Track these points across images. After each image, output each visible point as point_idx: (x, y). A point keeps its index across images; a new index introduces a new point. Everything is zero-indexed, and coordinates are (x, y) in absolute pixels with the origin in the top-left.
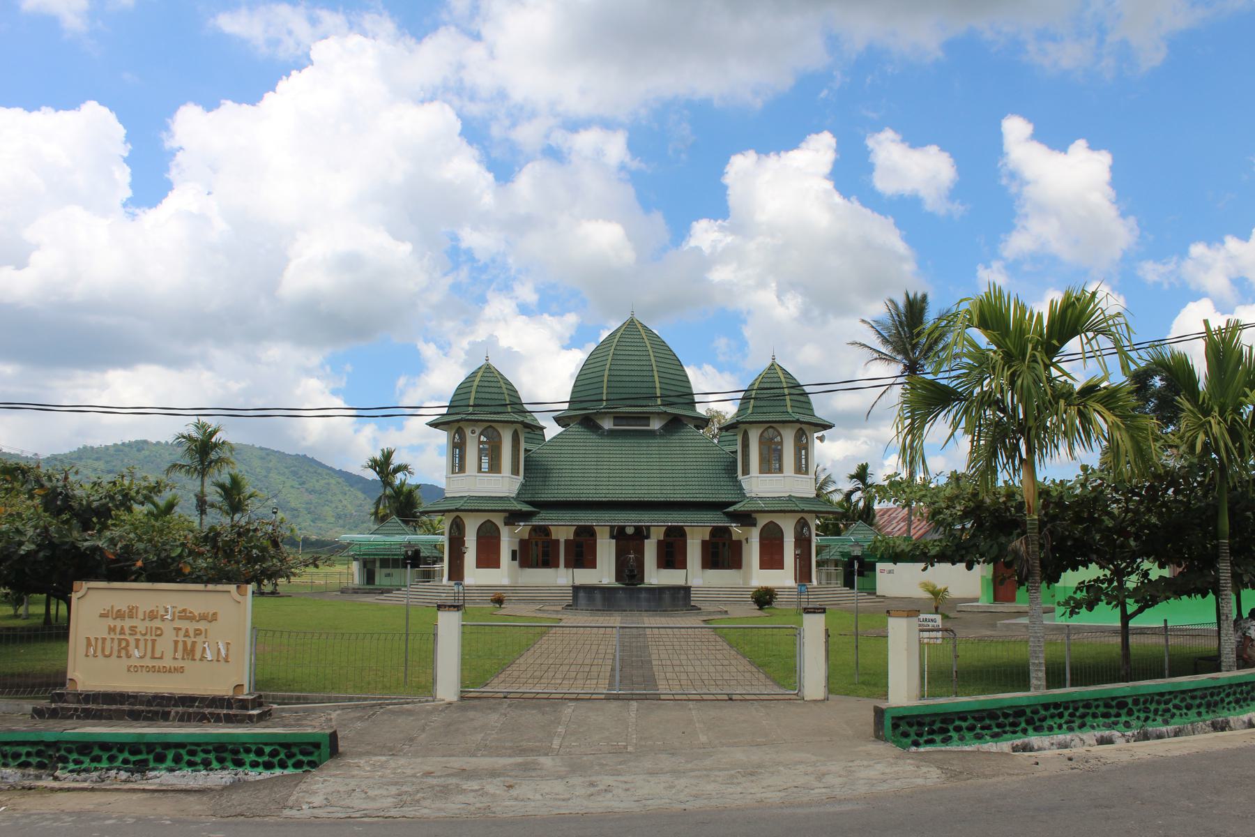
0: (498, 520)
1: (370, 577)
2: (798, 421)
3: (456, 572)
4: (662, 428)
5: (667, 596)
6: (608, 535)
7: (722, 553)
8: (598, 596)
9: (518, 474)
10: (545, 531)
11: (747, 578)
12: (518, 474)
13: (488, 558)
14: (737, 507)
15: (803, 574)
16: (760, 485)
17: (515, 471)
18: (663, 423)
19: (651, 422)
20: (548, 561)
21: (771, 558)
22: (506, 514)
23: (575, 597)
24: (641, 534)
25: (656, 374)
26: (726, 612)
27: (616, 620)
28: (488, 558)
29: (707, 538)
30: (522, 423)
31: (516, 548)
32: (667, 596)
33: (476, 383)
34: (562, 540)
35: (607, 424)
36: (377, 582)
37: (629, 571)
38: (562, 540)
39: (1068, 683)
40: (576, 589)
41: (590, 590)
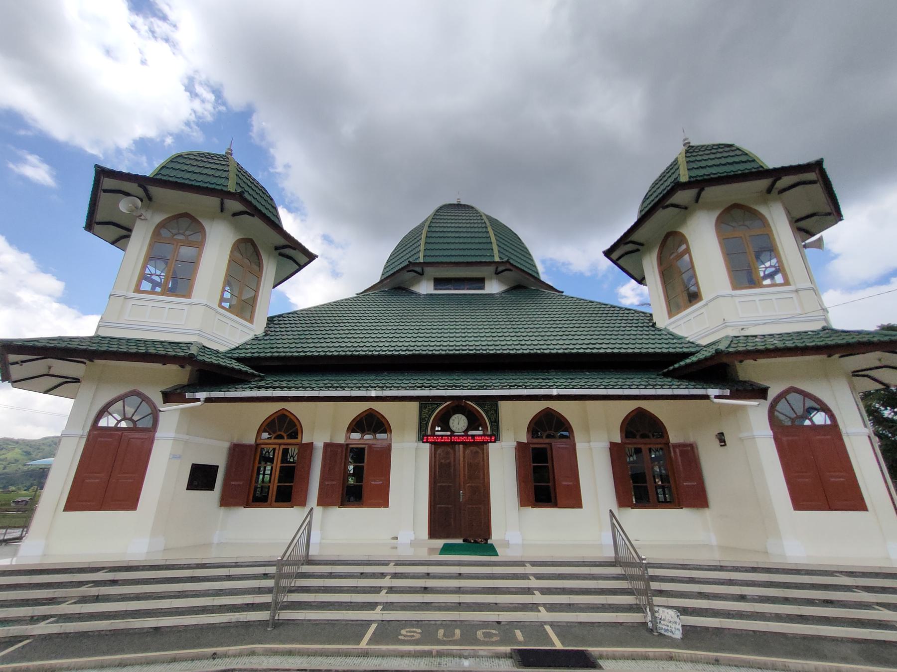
6: (413, 433)
7: (657, 474)
10: (284, 425)
20: (287, 493)
24: (484, 415)
29: (618, 440)
34: (319, 445)
38: (319, 445)
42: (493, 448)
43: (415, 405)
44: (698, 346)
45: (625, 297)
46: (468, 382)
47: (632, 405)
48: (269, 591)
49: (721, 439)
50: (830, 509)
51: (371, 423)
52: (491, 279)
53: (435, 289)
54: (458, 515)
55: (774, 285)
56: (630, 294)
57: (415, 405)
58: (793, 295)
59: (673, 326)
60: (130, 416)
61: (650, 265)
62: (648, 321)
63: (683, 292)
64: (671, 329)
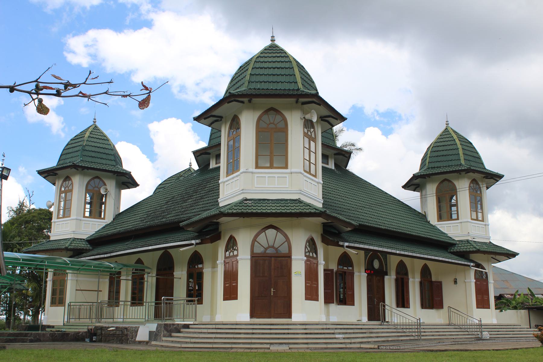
42: (386, 278)
43: (363, 252)
44: (454, 240)
45: (74, 52)
46: (422, 251)
47: (400, 258)
48: (423, 336)
49: (455, 282)
50: (484, 308)
51: (345, 260)
52: (241, 112)
54: (375, 312)
56: (412, 199)
57: (363, 252)
58: (484, 226)
59: (440, 226)
60: (267, 246)
61: (431, 189)
62: (422, 217)
63: (446, 209)
64: (438, 227)
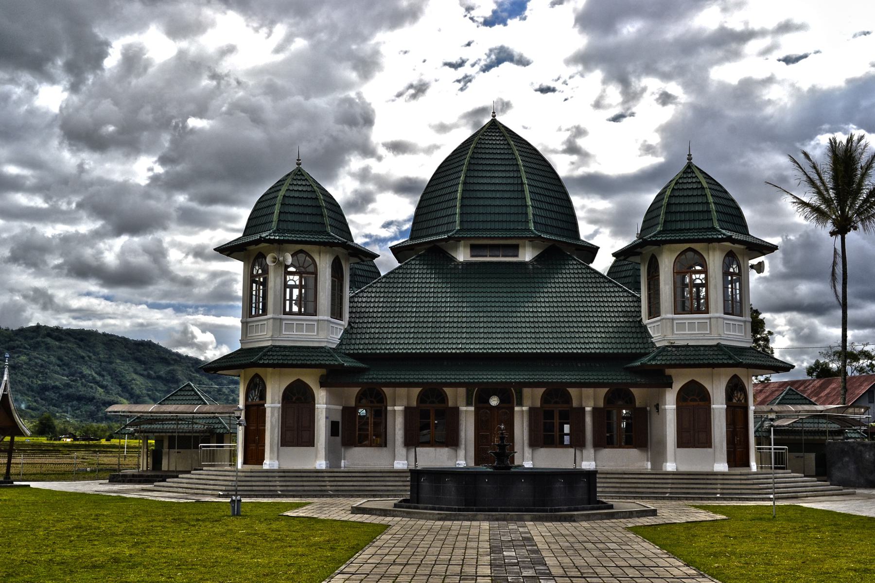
0: (311, 380)
1: (156, 457)
2: (729, 239)
3: (254, 454)
4: (537, 259)
5: (559, 485)
8: (451, 486)
9: (340, 317)
11: (659, 456)
12: (340, 317)
13: (298, 433)
14: (645, 360)
15: (737, 456)
16: (667, 329)
17: (337, 313)
18: (536, 253)
19: (521, 251)
21: (694, 434)
22: (323, 371)
23: (416, 488)
24: (510, 396)
25: (526, 187)
26: (653, 513)
27: (482, 529)
28: (298, 433)
30: (344, 245)
31: (338, 418)
32: (559, 485)
33: (281, 193)
35: (462, 256)
36: (165, 467)
37: (494, 446)
39: (397, 427)
40: (416, 475)
41: (437, 475)
53: (472, 256)
55: (705, 285)
